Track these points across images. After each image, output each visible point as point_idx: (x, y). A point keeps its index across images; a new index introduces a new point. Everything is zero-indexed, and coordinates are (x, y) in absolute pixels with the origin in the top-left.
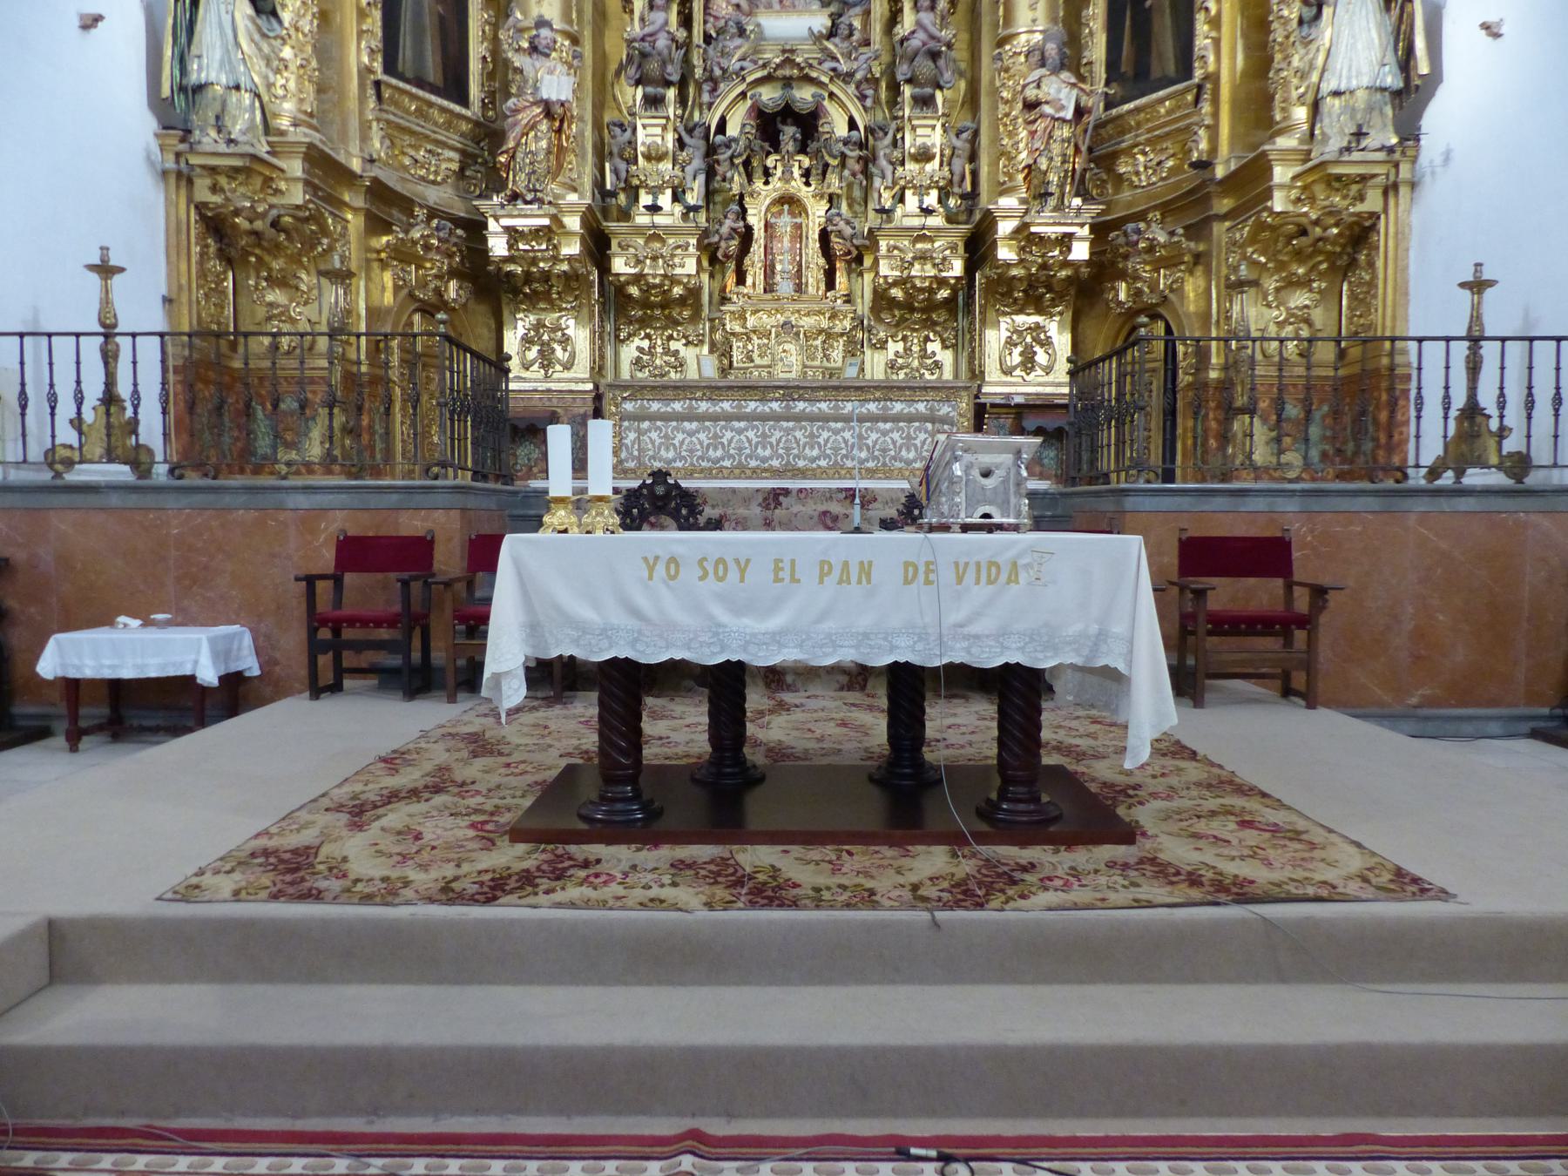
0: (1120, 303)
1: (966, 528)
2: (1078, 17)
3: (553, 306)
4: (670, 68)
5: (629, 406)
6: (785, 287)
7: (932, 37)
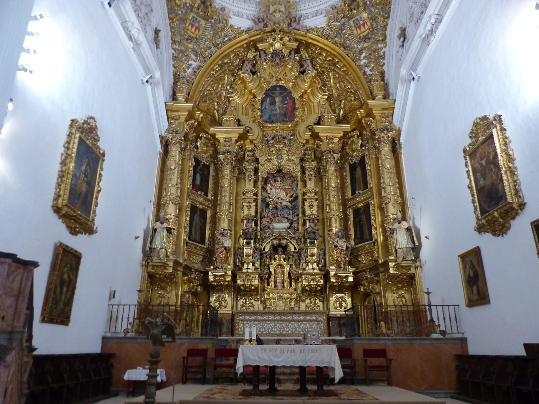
0: (362, 291)
1: (311, 344)
2: (347, 224)
3: (223, 292)
4: (252, 236)
5: (241, 318)
6: (280, 286)
7: (313, 229)
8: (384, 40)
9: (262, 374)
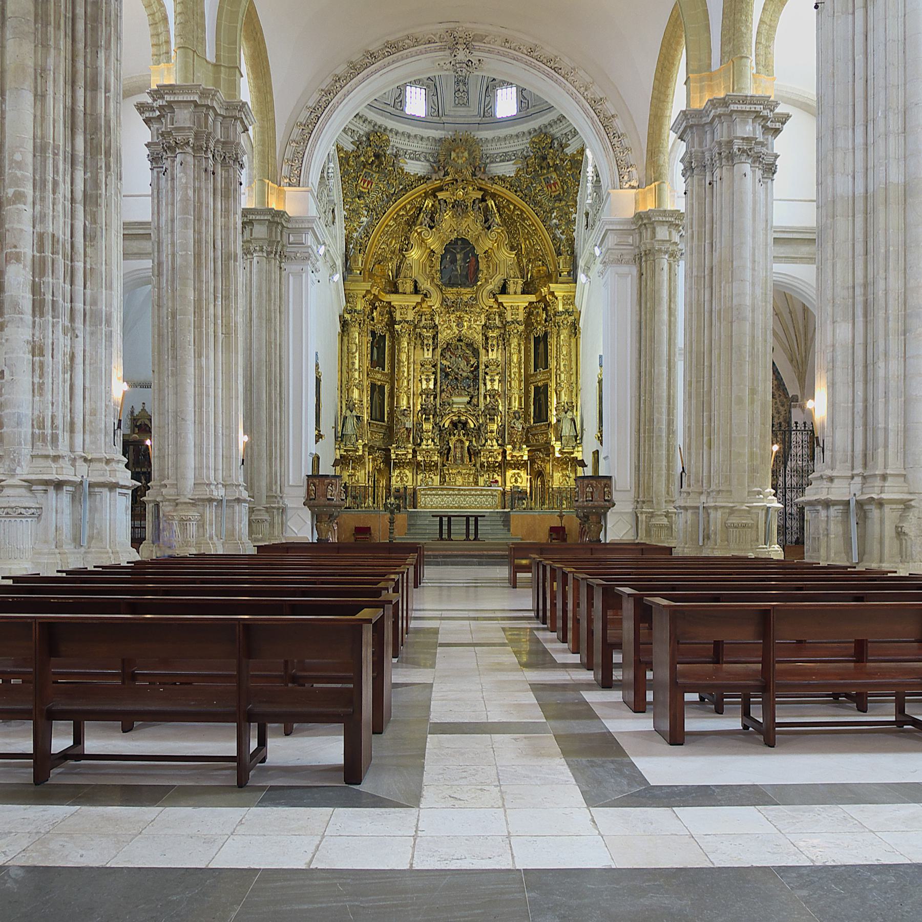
8: (575, 205)
9: (651, 709)
